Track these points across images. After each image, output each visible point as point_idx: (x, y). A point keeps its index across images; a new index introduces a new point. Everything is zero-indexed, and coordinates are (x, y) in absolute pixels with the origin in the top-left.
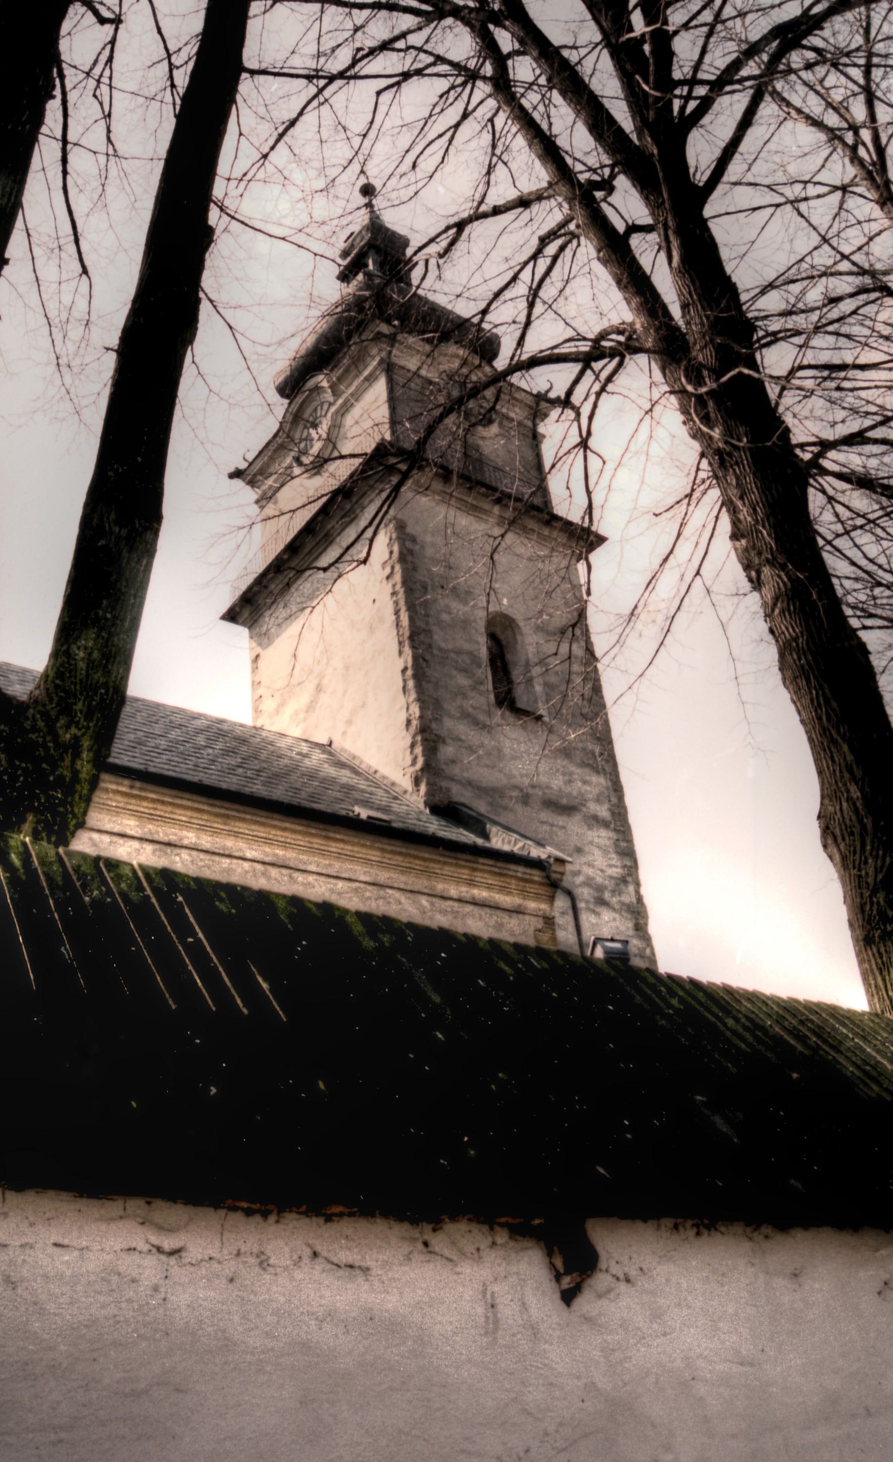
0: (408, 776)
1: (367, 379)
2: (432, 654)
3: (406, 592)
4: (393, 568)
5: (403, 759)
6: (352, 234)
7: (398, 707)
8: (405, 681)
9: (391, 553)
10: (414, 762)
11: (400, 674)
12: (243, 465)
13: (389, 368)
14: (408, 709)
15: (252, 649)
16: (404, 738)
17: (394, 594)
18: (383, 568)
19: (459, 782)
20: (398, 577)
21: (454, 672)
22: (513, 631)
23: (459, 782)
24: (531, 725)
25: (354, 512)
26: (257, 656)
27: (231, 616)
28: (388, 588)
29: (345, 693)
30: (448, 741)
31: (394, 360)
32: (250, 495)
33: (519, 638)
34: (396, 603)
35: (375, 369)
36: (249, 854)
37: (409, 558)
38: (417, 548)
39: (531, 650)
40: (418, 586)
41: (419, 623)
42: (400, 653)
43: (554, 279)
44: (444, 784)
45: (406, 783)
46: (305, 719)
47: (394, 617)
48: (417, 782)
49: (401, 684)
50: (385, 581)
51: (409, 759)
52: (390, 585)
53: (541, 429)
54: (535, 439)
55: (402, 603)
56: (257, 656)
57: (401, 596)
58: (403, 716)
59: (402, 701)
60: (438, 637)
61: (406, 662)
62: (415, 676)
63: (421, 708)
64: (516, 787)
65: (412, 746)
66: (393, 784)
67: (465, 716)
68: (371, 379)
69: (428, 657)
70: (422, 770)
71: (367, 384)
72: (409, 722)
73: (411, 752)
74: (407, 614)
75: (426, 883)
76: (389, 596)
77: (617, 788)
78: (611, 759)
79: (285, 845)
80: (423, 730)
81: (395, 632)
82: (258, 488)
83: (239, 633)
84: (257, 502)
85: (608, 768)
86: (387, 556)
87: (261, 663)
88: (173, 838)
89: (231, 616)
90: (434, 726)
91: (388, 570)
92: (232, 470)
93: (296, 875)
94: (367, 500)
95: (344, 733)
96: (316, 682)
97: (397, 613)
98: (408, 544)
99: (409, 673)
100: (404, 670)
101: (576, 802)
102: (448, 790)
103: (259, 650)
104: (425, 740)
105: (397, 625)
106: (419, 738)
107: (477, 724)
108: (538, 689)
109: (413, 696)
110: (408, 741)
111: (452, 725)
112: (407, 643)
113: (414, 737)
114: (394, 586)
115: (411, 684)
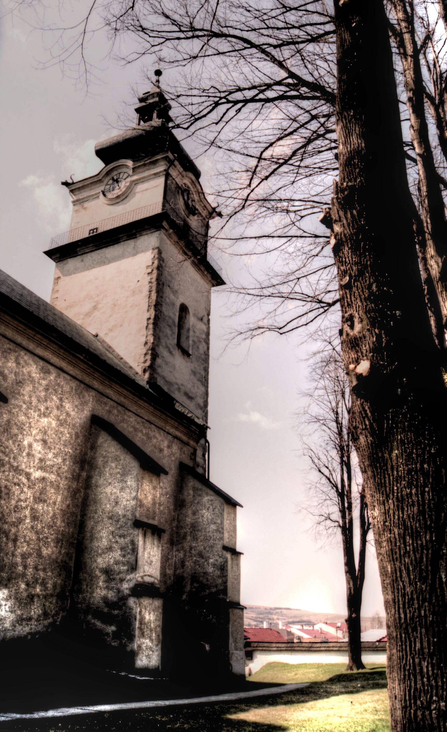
0: (140, 367)
1: (155, 174)
2: (161, 315)
3: (157, 284)
4: (152, 270)
5: (139, 358)
6: (149, 92)
7: (142, 334)
8: (148, 324)
9: (153, 263)
10: (145, 362)
11: (146, 320)
12: (70, 181)
13: (167, 175)
14: (147, 337)
15: (55, 273)
16: (142, 349)
17: (150, 282)
18: (147, 268)
19: (160, 376)
20: (154, 275)
21: (167, 326)
22: (186, 313)
23: (160, 376)
24: (186, 357)
25: (136, 235)
26: (59, 278)
27: (50, 253)
28: (148, 278)
29: (111, 316)
30: (160, 357)
31: (170, 171)
32: (70, 198)
33: (187, 316)
34: (151, 287)
35: (161, 172)
36: (114, 397)
37: (161, 269)
38: (164, 265)
39: (191, 324)
40: (161, 283)
41: (159, 300)
42: (148, 310)
43: (291, 194)
44: (156, 375)
45: (139, 370)
46: (83, 319)
47: (148, 293)
48: (145, 371)
49: (146, 325)
50: (146, 275)
51: (142, 360)
52: (149, 278)
53: (211, 222)
54: (207, 227)
55: (154, 289)
56: (59, 278)
57: (154, 284)
58: (143, 340)
59: (144, 332)
60: (164, 309)
61: (150, 315)
62: (154, 324)
63: (154, 339)
64: (177, 384)
65: (146, 354)
66: (131, 367)
67: (167, 347)
68: (156, 175)
69: (160, 317)
70: (149, 367)
71: (154, 176)
72: (146, 343)
73: (144, 357)
74: (156, 294)
75: (164, 425)
76: (148, 283)
77: (207, 394)
78: (207, 380)
79: (125, 397)
80: (153, 349)
81: (147, 300)
82: (75, 195)
83: (51, 263)
84: (73, 202)
85: (206, 384)
86: (150, 264)
87: (60, 281)
88: (91, 384)
89: (50, 253)
90: (157, 348)
91: (149, 270)
92: (64, 181)
93: (126, 411)
94: (144, 233)
95: (106, 334)
96: (94, 304)
97: (150, 291)
98: (161, 262)
99: (151, 321)
100: (149, 319)
101: (193, 396)
102: (156, 378)
103: (60, 274)
104: (152, 354)
105: (149, 297)
106: (150, 352)
107: (171, 353)
108: (191, 342)
109: (151, 332)
110: (144, 351)
111: (162, 351)
112: (153, 307)
113: (147, 350)
114: (151, 279)
115: (151, 326)
